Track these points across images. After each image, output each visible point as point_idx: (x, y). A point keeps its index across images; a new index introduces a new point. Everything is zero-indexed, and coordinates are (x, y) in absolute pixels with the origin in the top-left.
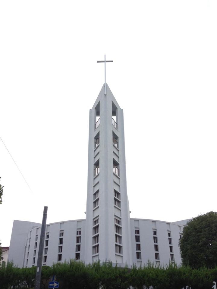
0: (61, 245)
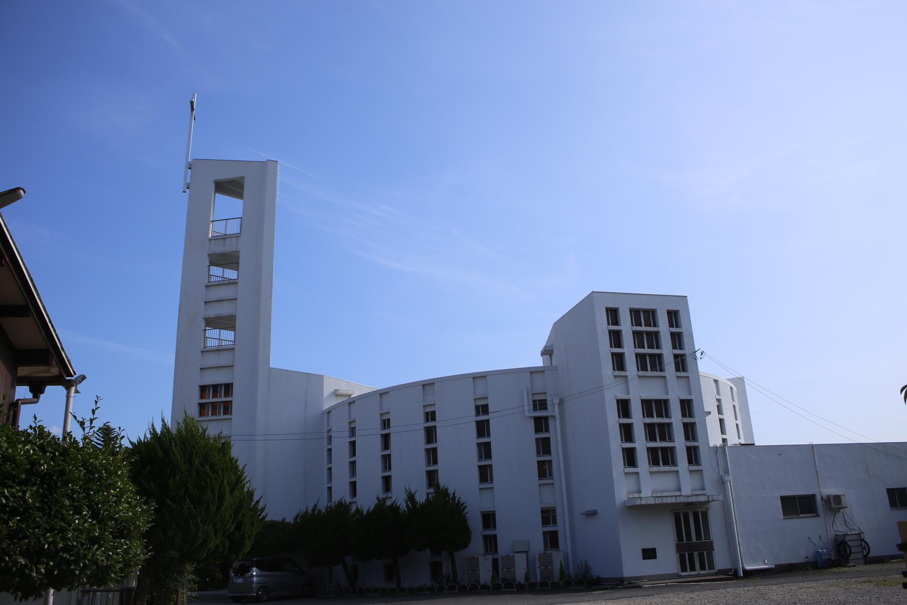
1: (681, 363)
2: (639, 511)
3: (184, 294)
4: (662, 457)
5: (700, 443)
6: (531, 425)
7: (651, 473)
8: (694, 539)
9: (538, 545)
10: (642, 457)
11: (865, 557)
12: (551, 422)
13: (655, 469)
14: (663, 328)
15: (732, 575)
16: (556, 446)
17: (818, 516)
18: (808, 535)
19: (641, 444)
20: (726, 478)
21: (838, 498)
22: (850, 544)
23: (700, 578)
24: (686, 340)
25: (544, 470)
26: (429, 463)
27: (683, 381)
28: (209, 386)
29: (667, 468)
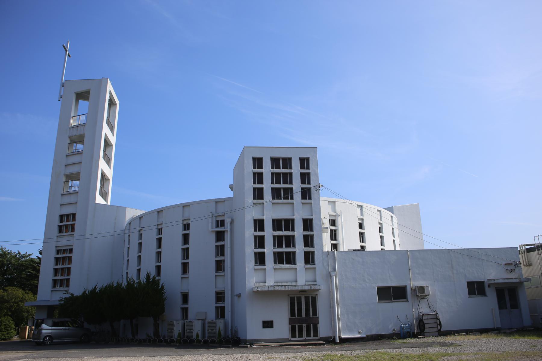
0: (159, 250)
1: (306, 194)
2: (266, 295)
3: (55, 162)
4: (285, 259)
5: (315, 249)
6: (213, 237)
7: (274, 269)
8: (304, 315)
9: (212, 315)
10: (269, 259)
11: (439, 331)
12: (225, 234)
13: (278, 266)
14: (296, 170)
15: (330, 341)
16: (227, 250)
17: (407, 301)
18: (400, 313)
19: (269, 249)
20: (332, 274)
21: (422, 289)
22: (425, 322)
23: (317, 342)
24: (312, 177)
25: (219, 266)
26: (184, 258)
27: (308, 206)
28: (65, 215)
29: (288, 266)
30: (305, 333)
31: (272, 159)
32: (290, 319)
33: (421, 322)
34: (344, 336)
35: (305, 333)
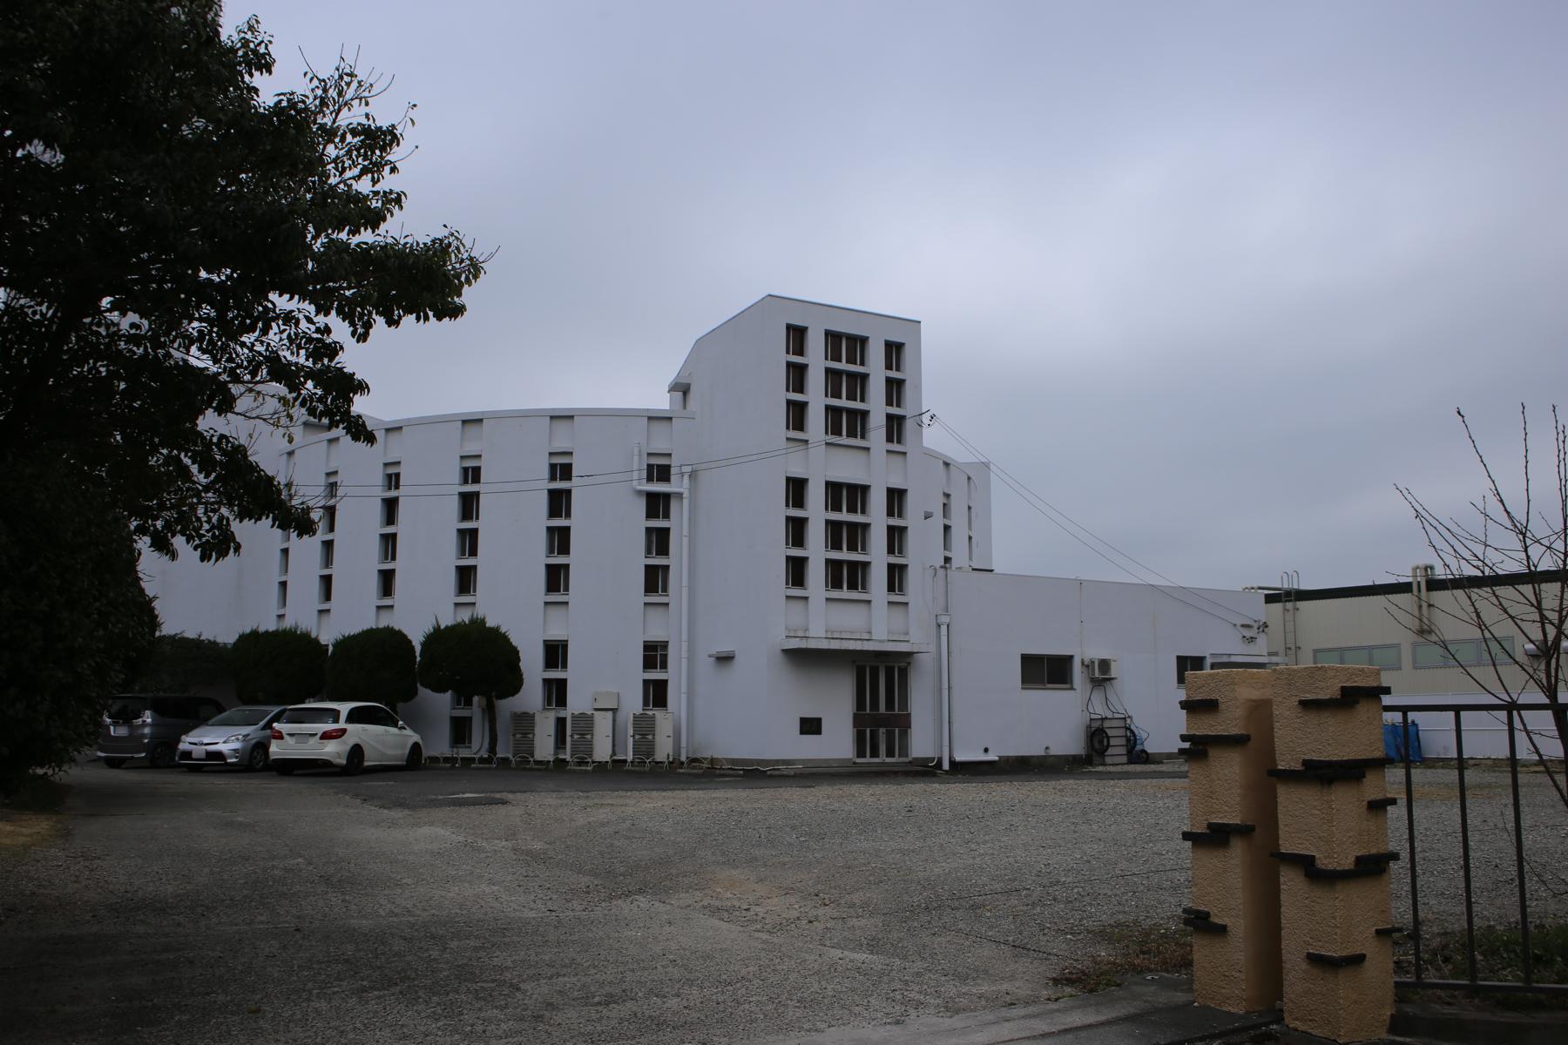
0: (390, 530)
10: (816, 573)
29: (854, 595)
30: (883, 748)
31: (828, 333)
32: (855, 716)
33: (1097, 736)
34: (959, 758)
35: (883, 748)
